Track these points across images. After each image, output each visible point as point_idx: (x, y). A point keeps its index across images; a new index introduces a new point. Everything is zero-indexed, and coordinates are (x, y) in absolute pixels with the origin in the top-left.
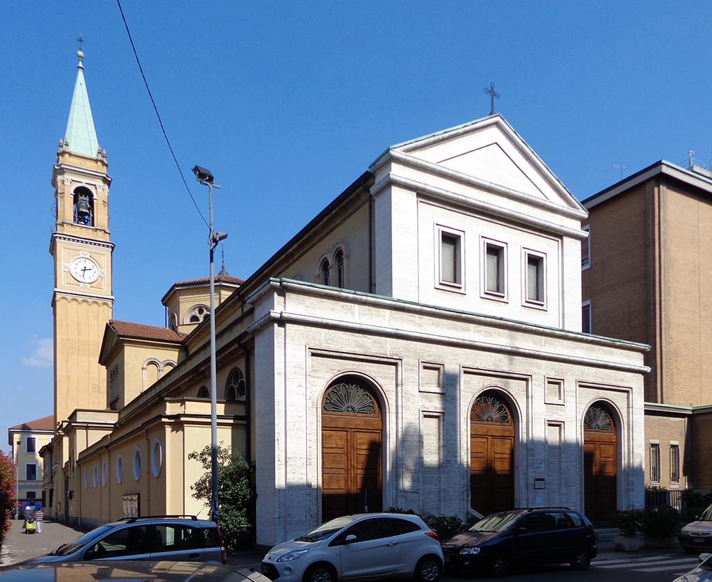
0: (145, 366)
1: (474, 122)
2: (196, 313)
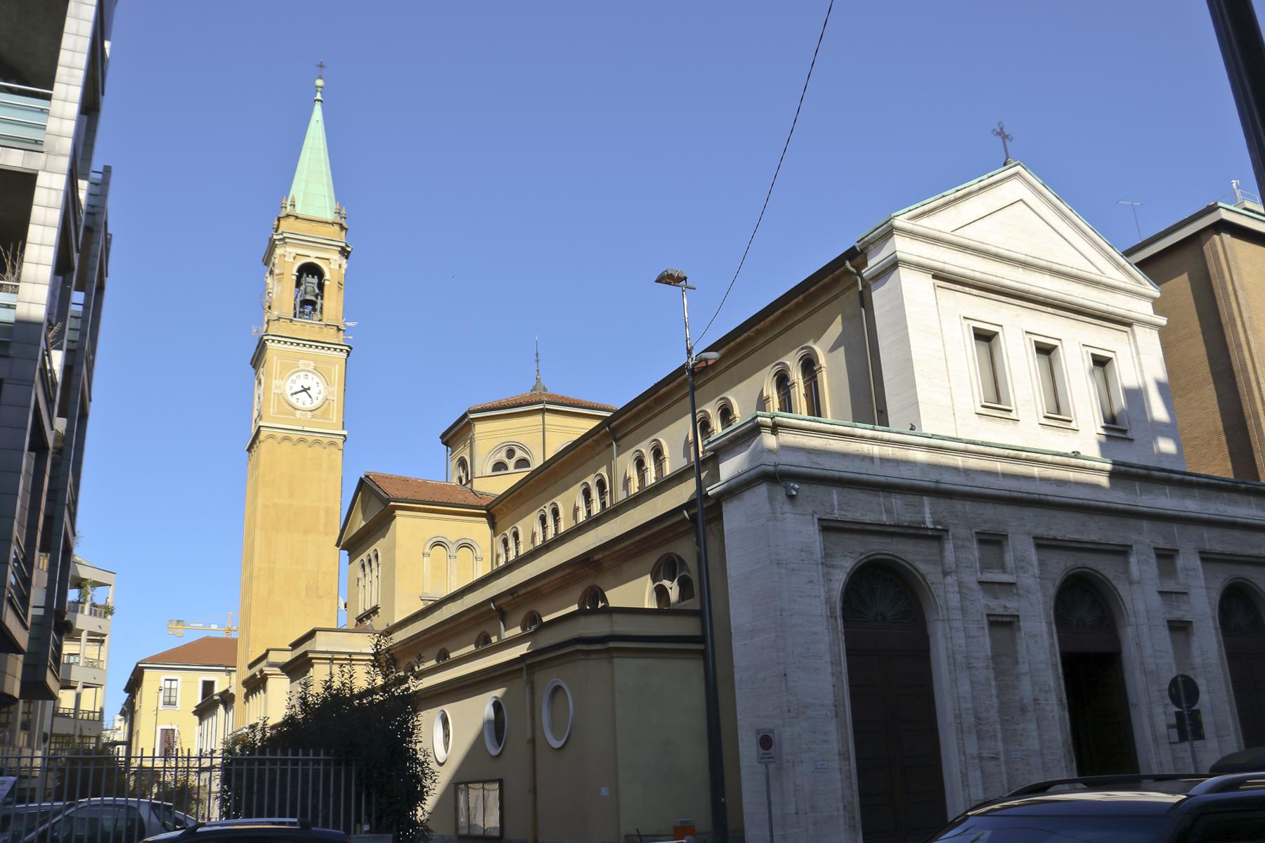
0: (427, 550)
1: (990, 174)
2: (519, 454)
